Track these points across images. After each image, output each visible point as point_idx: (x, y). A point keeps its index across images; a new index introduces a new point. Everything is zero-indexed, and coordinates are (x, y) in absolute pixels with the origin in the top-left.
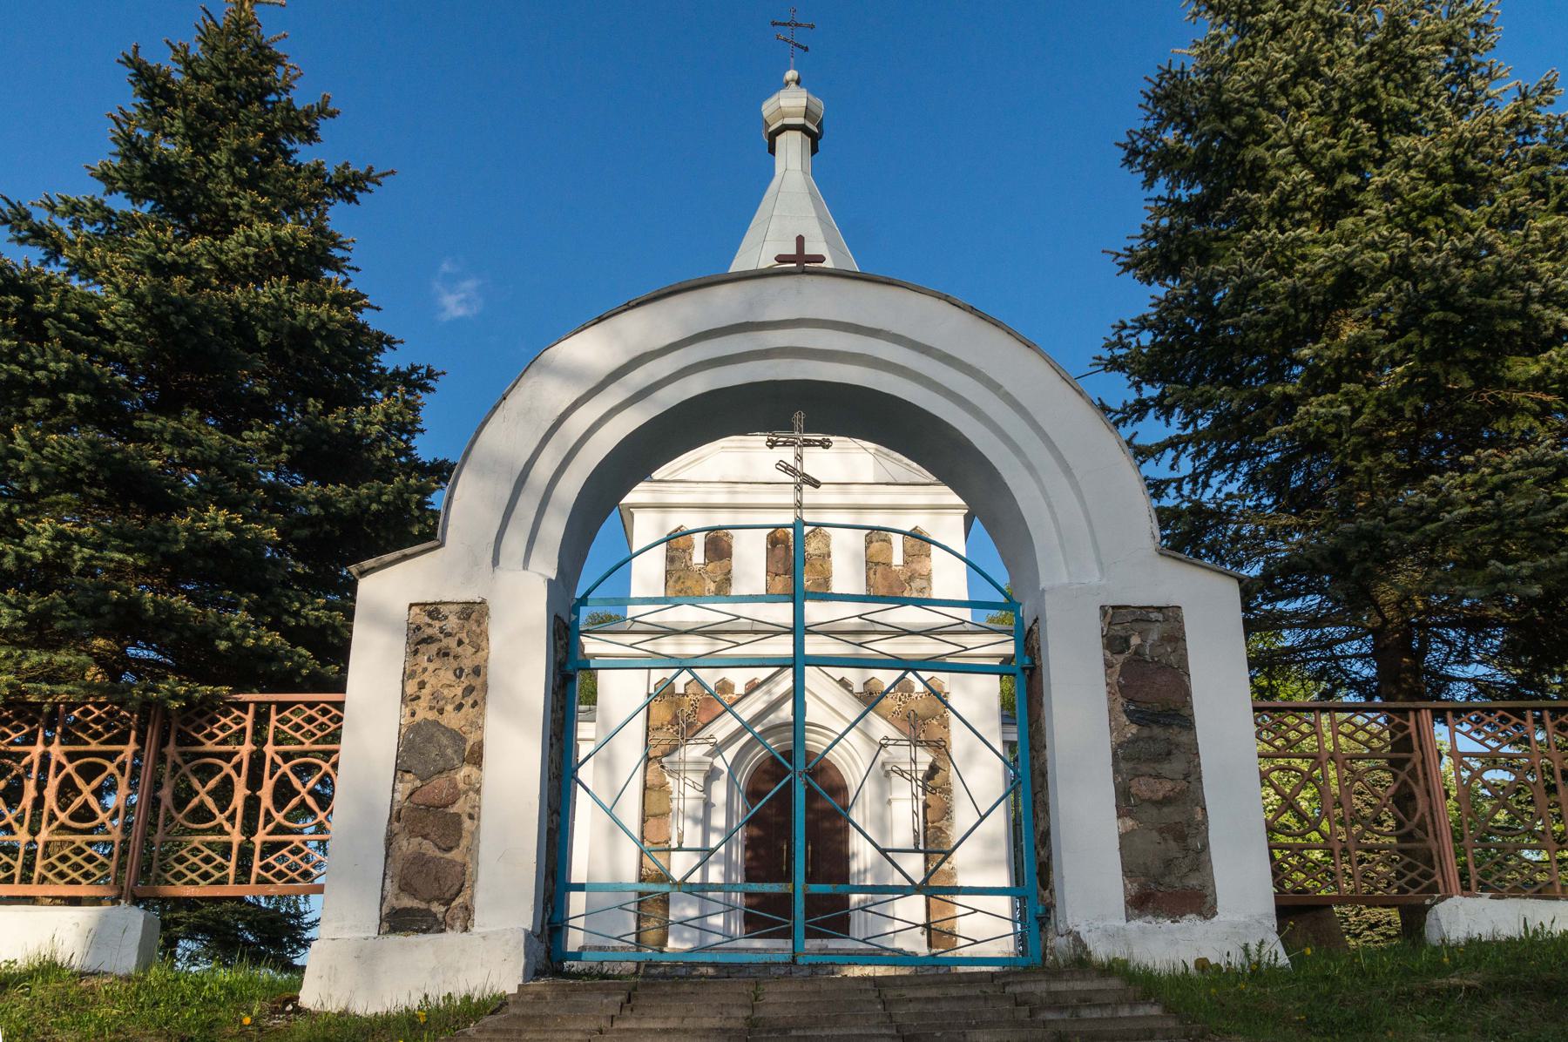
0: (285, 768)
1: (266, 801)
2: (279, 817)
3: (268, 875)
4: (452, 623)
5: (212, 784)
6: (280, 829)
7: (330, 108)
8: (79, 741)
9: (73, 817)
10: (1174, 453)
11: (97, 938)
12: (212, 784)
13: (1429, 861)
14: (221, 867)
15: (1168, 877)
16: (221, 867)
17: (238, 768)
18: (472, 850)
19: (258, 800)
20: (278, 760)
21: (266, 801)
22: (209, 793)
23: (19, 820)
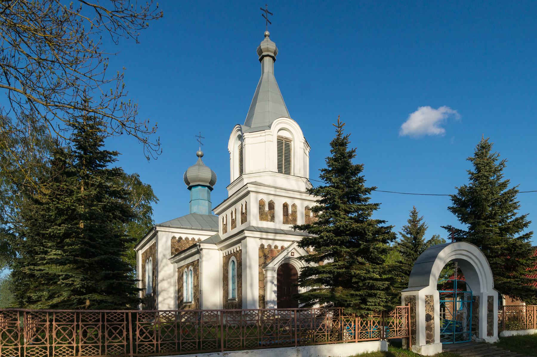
0: (110, 328)
1: (54, 336)
2: (58, 340)
3: (58, 354)
4: (429, 298)
5: (117, 331)
6: (142, 341)
7: (470, 175)
8: (60, 321)
9: (144, 338)
10: (157, 227)
11: (382, 346)
12: (117, 331)
13: (338, 340)
14: (214, 346)
15: (490, 334)
16: (97, 351)
17: (123, 327)
18: (434, 332)
19: (136, 334)
20: (108, 326)
21: (54, 336)
22: (117, 333)
23: (123, 339)
